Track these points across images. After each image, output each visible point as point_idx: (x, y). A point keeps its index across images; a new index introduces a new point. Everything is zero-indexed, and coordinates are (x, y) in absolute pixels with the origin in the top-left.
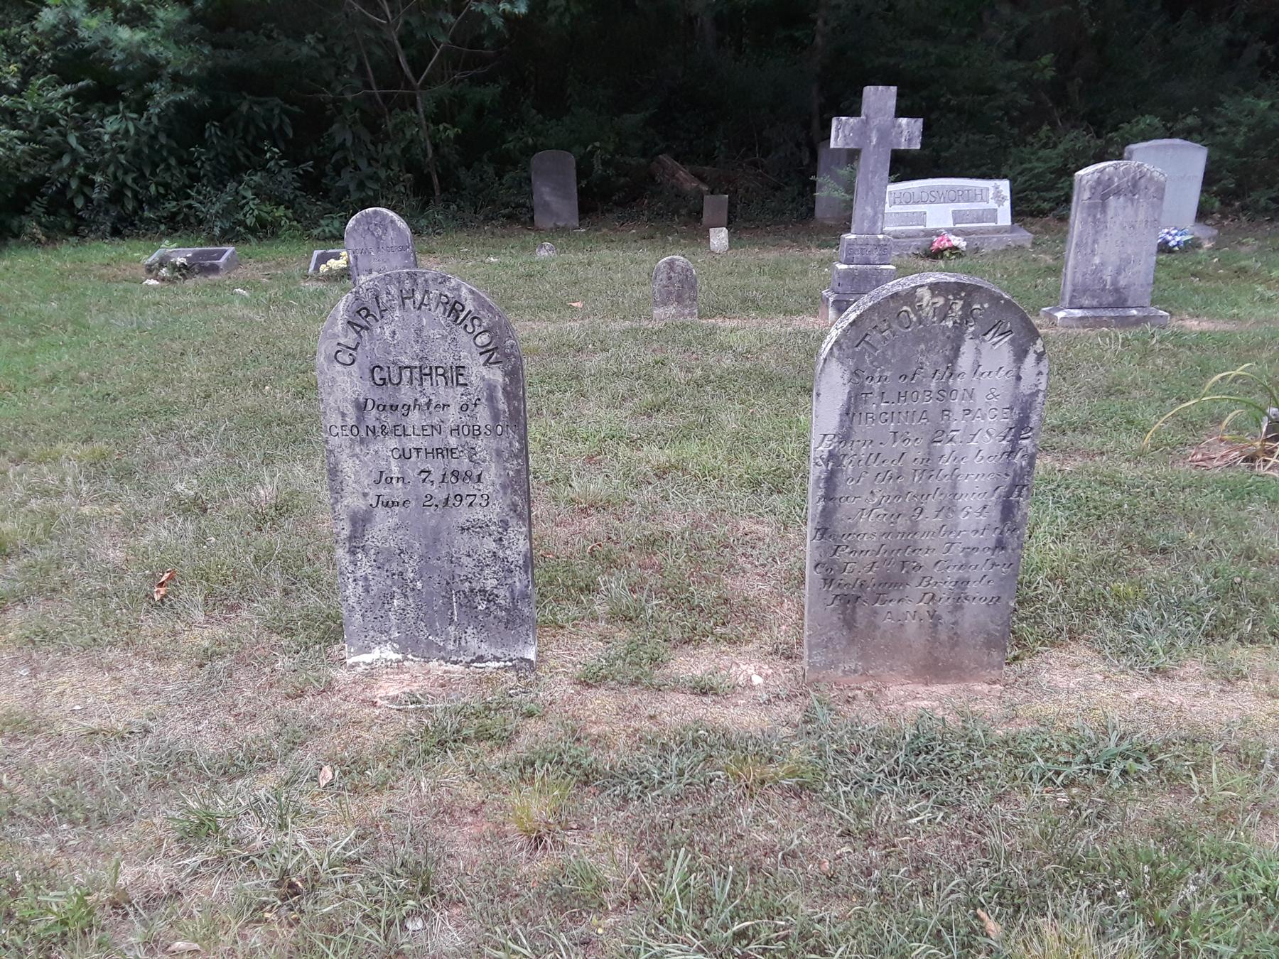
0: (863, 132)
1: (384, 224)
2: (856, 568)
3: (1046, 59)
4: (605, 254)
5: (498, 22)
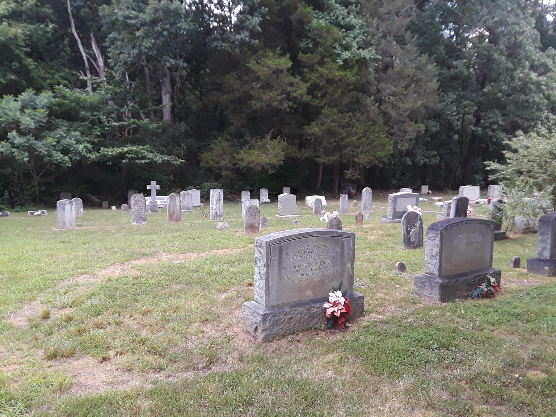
0: (152, 187)
1: (78, 200)
2: (171, 213)
3: (172, 176)
4: (89, 211)
5: (66, 168)
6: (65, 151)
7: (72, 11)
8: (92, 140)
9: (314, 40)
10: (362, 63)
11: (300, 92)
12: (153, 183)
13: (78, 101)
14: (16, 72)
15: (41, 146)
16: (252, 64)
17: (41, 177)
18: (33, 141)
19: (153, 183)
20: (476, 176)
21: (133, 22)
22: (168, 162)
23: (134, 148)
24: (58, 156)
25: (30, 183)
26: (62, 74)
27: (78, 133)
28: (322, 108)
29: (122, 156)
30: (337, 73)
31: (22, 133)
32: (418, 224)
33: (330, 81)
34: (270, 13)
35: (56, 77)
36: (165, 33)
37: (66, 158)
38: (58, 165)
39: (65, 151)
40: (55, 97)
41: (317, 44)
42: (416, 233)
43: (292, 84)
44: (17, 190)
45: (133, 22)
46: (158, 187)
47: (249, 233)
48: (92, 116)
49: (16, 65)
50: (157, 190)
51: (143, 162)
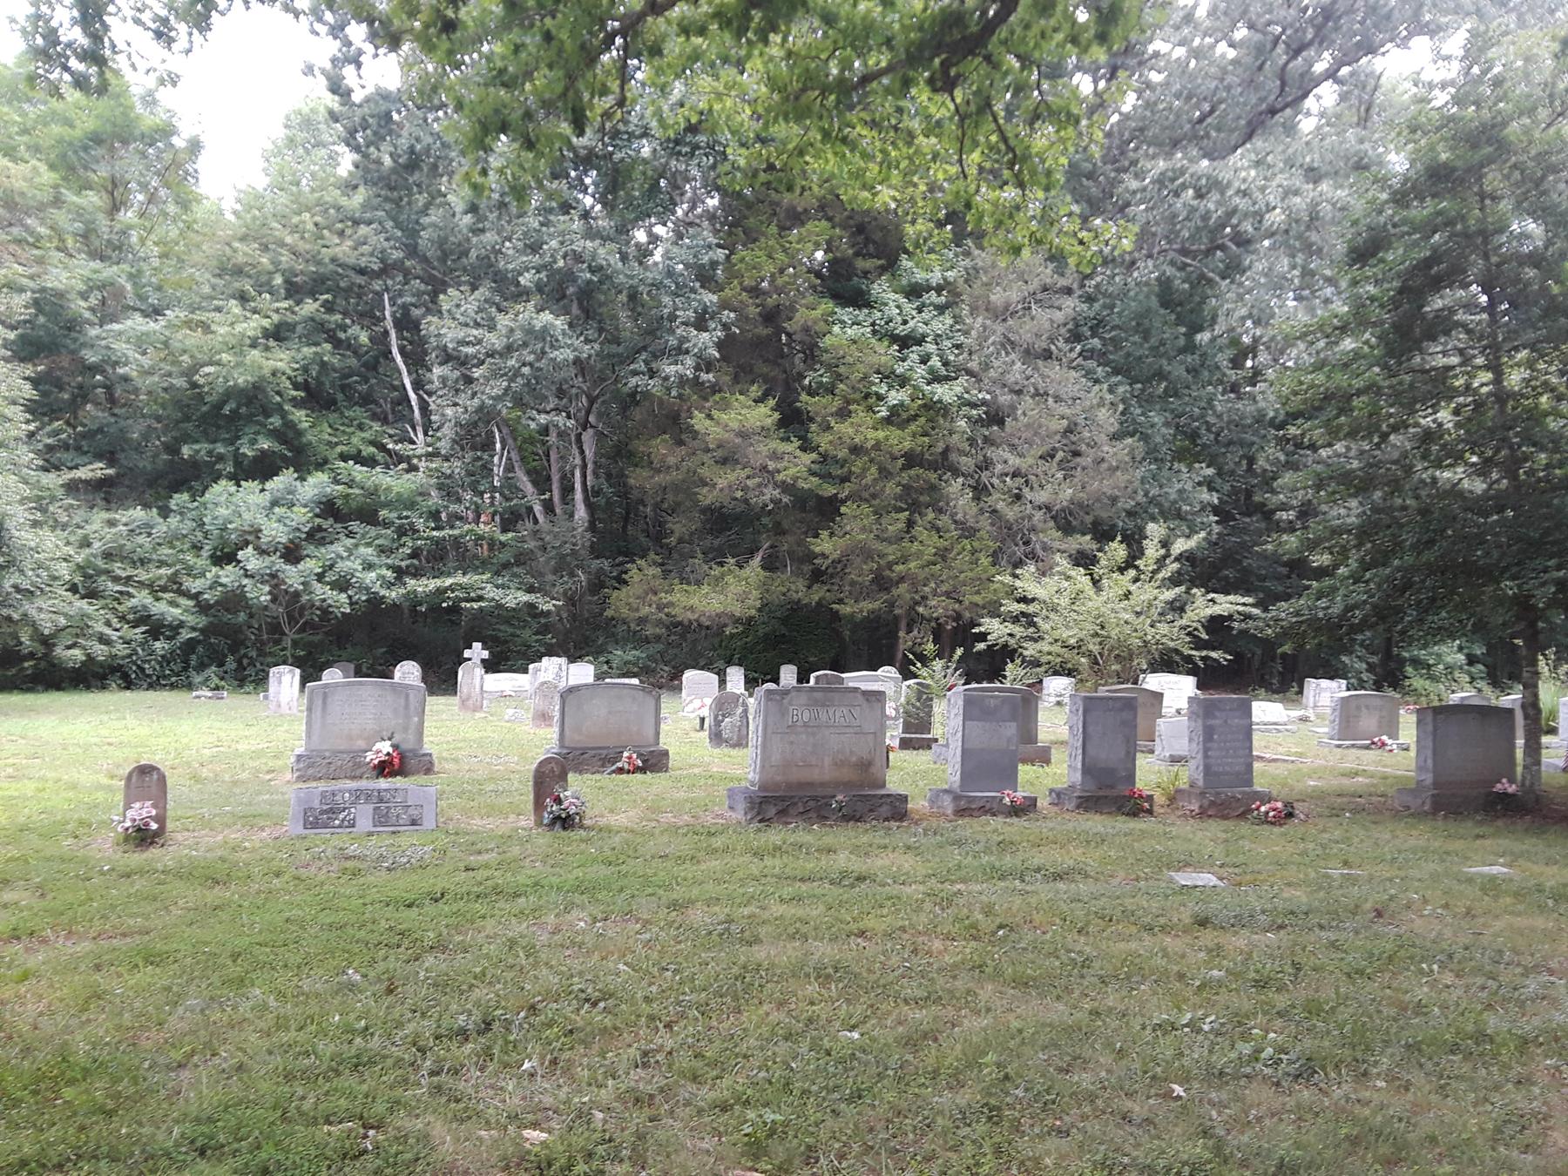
6: (342, 585)
7: (393, 314)
8: (397, 563)
9: (830, 367)
10: (935, 409)
11: (792, 471)
12: (477, 645)
13: (373, 492)
14: (276, 434)
15: (293, 576)
16: (699, 421)
17: (302, 630)
18: (280, 564)
19: (477, 645)
20: (1344, 658)
21: (470, 350)
22: (531, 606)
23: (464, 580)
24: (322, 592)
25: (277, 642)
26: (366, 435)
27: (370, 550)
28: (843, 502)
29: (440, 592)
30: (871, 434)
31: (262, 552)
32: (740, 710)
33: (856, 450)
34: (743, 318)
35: (355, 440)
36: (526, 370)
37: (343, 597)
38: (325, 612)
39: (342, 585)
40: (336, 482)
41: (839, 378)
42: (733, 726)
43: (775, 456)
44: (254, 654)
45: (470, 350)
46: (485, 654)
47: (538, 726)
48: (400, 518)
49: (275, 421)
50: (483, 661)
51: (475, 605)
